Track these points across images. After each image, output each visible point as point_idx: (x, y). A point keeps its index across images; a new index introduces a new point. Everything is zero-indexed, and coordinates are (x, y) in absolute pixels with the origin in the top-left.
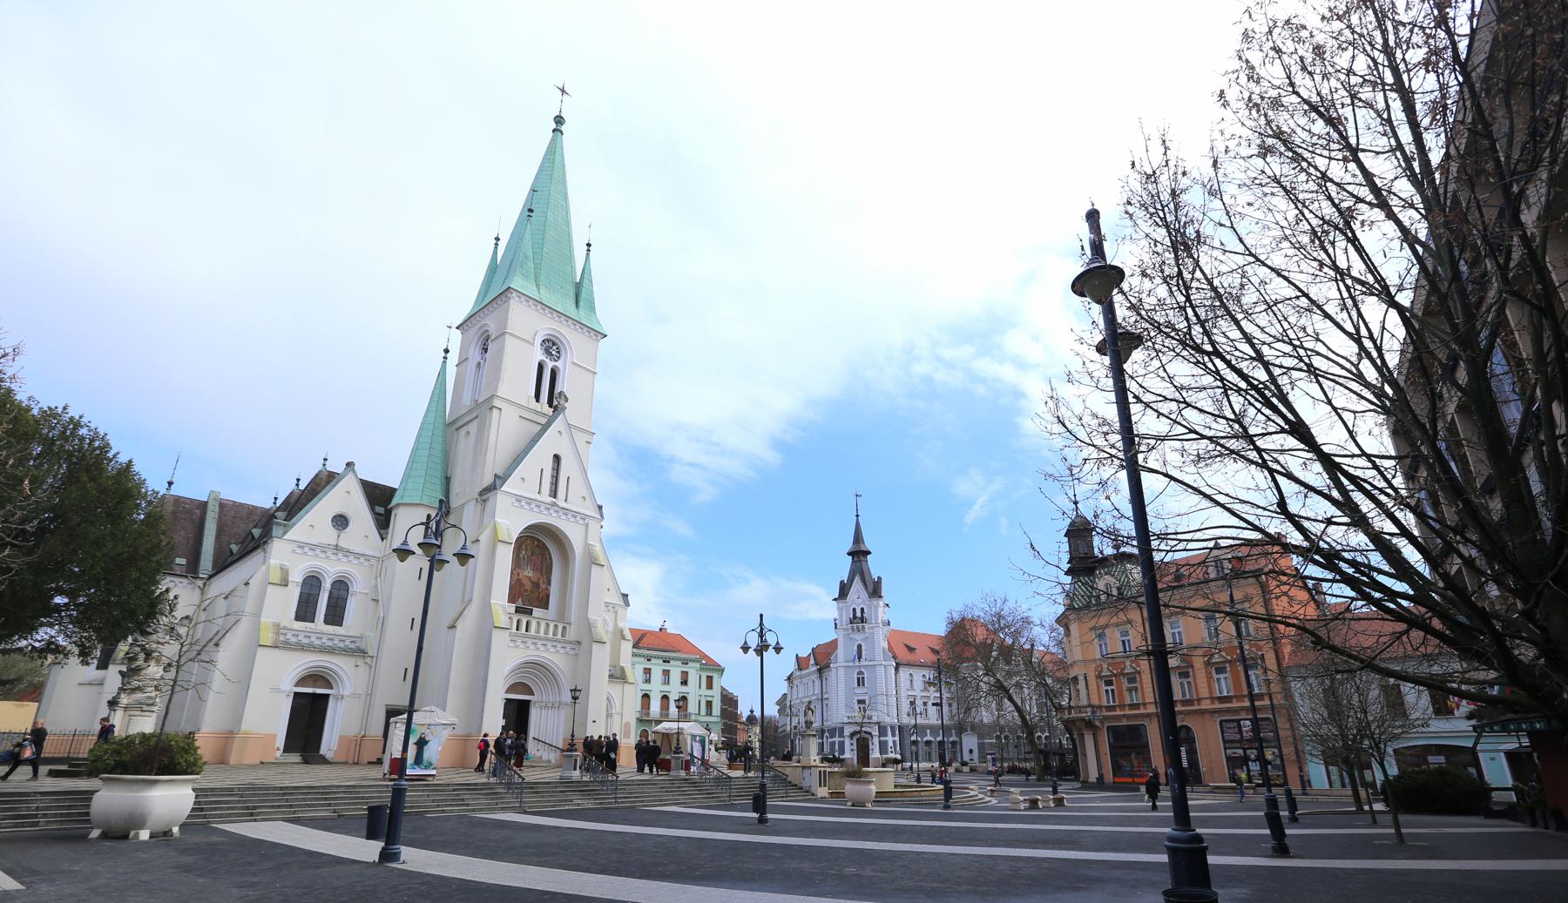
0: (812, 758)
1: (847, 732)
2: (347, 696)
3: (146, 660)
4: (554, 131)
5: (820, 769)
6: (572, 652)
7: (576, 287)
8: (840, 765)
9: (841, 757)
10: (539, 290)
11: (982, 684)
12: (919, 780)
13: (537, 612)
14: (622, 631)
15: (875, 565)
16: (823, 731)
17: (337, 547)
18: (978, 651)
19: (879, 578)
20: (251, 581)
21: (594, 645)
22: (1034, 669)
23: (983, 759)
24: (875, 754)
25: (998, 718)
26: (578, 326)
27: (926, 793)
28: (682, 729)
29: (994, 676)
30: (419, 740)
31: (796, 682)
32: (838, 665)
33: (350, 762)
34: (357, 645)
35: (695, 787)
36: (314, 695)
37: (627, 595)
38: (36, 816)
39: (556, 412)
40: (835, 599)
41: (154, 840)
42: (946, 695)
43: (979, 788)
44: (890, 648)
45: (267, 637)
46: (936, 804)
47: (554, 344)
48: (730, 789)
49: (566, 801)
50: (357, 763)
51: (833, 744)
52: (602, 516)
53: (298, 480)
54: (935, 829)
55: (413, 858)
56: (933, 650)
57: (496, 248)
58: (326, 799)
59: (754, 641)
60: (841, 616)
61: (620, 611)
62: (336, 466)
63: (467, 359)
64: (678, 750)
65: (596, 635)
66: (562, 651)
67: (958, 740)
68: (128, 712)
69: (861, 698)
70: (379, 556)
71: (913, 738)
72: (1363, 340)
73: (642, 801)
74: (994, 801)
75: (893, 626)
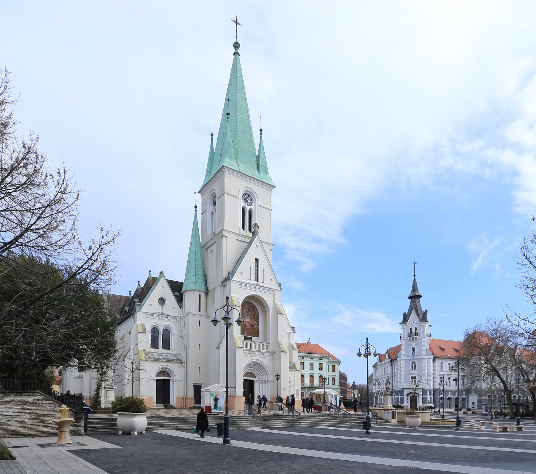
0: (389, 405)
1: (405, 392)
2: (177, 380)
3: (107, 368)
4: (234, 54)
5: (393, 411)
6: (272, 357)
7: (257, 159)
8: (401, 409)
9: (402, 405)
10: (238, 165)
11: (483, 368)
12: (443, 417)
13: (254, 339)
14: (293, 346)
15: (424, 304)
16: (392, 392)
17: (163, 314)
18: (482, 350)
19: (426, 311)
20: (131, 332)
21: (282, 353)
22: (515, 360)
23: (480, 407)
24: (420, 404)
25: (491, 386)
26: (260, 183)
27: (447, 423)
28: (326, 392)
29: (490, 363)
30: (215, 398)
31: (378, 368)
32: (401, 358)
33: (182, 407)
34: (177, 357)
35: (334, 418)
36: (164, 380)
38: (96, 427)
39: (254, 235)
40: (401, 323)
41: (139, 435)
42: (461, 374)
43: (476, 422)
44: (431, 349)
45: (142, 357)
46: (452, 428)
47: (249, 196)
48: (350, 419)
49: (278, 423)
50: (185, 408)
51: (397, 399)
52: (281, 289)
54: (451, 438)
55: (234, 443)
56: (456, 350)
57: (212, 141)
58: (186, 422)
59: (363, 351)
60: (404, 332)
61: (291, 336)
62: (156, 275)
63: (206, 210)
64: (324, 402)
65: (283, 348)
66: (267, 357)
67: (466, 397)
68: (106, 389)
69: (413, 376)
70: (180, 316)
71: (442, 396)
73: (311, 424)
74: (483, 428)
75: (433, 337)
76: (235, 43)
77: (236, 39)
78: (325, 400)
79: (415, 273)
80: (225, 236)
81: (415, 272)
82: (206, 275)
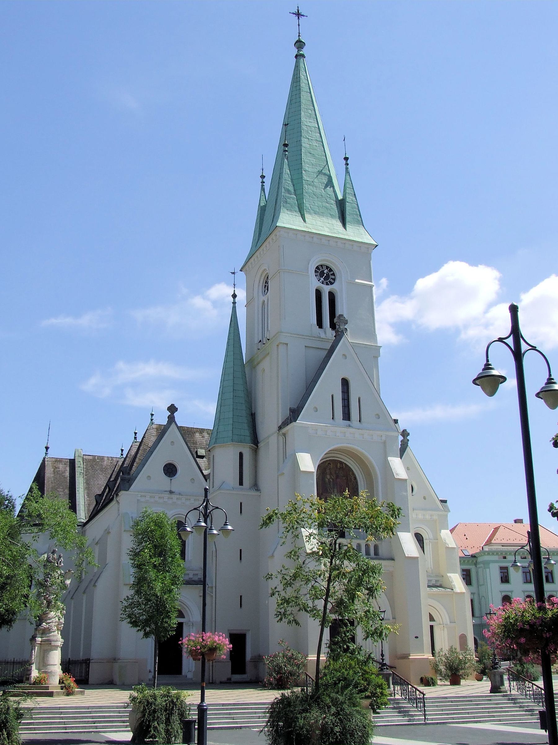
4: (296, 56)
37: (445, 502)
50: (212, 683)
53: (136, 433)
72: (447, 620)
76: (297, 42)
77: (299, 36)
80: (284, 343)
82: (255, 413)
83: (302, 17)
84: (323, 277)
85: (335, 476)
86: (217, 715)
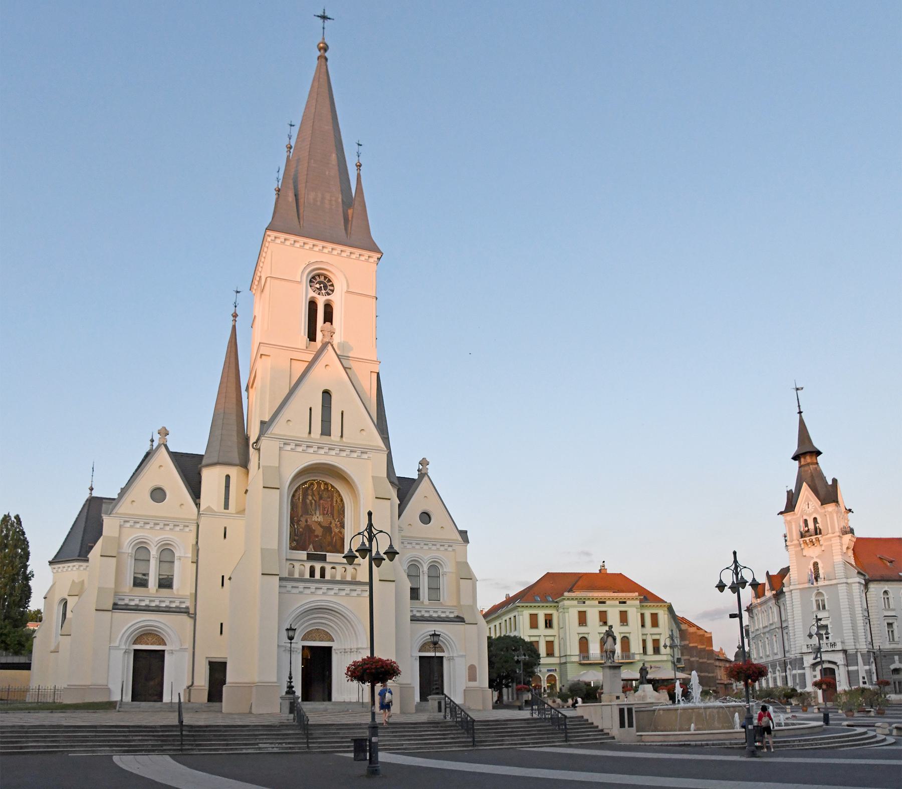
13: (330, 557)
15: (828, 466)
16: (785, 663)
19: (835, 481)
32: (792, 587)
40: (781, 513)
78: (292, 684)
79: (799, 409)
81: (799, 406)
83: (328, 20)
84: (323, 289)
85: (317, 497)
86: (76, 747)
